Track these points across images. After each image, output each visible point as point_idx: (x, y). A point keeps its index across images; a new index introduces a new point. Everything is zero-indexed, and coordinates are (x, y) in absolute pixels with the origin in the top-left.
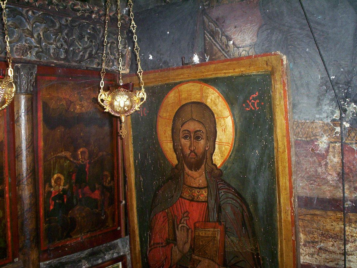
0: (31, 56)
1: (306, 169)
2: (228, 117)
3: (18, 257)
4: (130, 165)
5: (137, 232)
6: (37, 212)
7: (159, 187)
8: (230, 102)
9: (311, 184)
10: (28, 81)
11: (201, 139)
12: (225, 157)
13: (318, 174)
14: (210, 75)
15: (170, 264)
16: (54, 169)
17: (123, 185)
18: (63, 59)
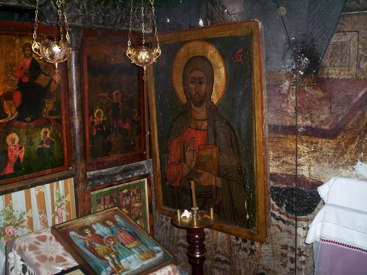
0: (78, 23)
1: (274, 105)
2: (221, 67)
3: (71, 166)
4: (152, 104)
5: (158, 155)
6: (84, 136)
7: (174, 121)
8: (224, 57)
9: (278, 116)
10: (77, 41)
11: (204, 84)
12: (219, 97)
13: (282, 108)
14: (210, 35)
15: (181, 177)
16: (96, 105)
17: (148, 120)
18: (102, 24)
